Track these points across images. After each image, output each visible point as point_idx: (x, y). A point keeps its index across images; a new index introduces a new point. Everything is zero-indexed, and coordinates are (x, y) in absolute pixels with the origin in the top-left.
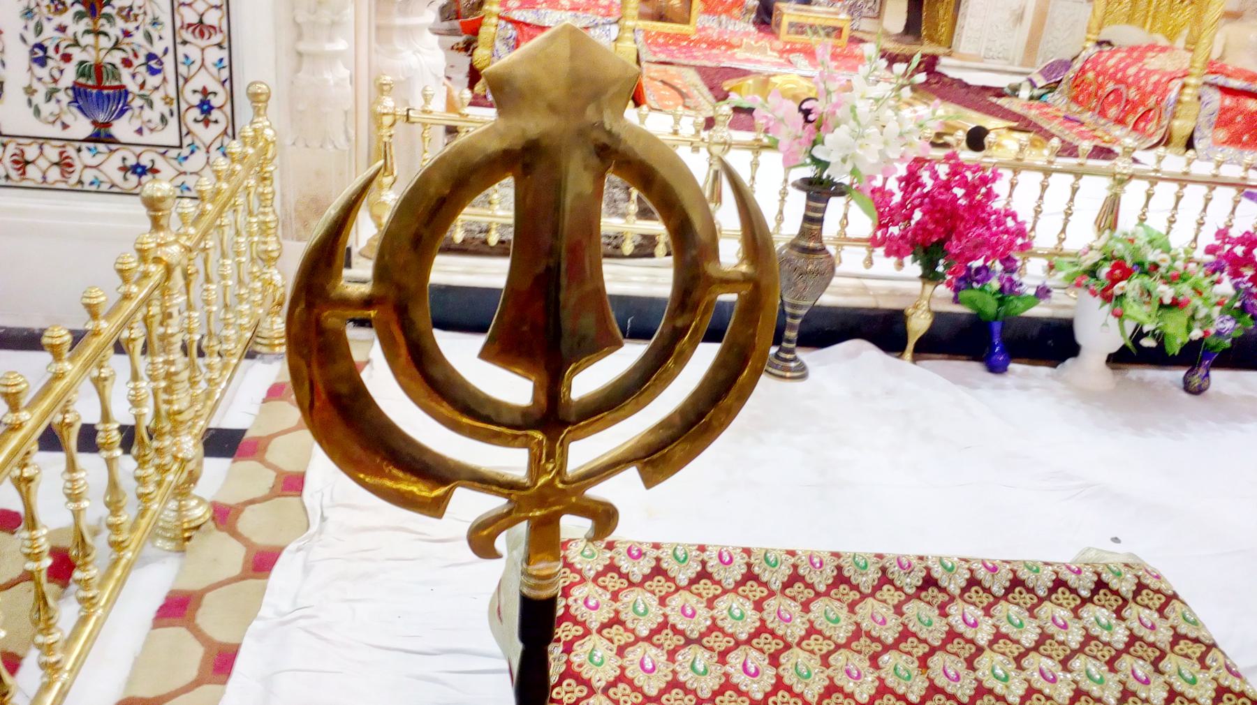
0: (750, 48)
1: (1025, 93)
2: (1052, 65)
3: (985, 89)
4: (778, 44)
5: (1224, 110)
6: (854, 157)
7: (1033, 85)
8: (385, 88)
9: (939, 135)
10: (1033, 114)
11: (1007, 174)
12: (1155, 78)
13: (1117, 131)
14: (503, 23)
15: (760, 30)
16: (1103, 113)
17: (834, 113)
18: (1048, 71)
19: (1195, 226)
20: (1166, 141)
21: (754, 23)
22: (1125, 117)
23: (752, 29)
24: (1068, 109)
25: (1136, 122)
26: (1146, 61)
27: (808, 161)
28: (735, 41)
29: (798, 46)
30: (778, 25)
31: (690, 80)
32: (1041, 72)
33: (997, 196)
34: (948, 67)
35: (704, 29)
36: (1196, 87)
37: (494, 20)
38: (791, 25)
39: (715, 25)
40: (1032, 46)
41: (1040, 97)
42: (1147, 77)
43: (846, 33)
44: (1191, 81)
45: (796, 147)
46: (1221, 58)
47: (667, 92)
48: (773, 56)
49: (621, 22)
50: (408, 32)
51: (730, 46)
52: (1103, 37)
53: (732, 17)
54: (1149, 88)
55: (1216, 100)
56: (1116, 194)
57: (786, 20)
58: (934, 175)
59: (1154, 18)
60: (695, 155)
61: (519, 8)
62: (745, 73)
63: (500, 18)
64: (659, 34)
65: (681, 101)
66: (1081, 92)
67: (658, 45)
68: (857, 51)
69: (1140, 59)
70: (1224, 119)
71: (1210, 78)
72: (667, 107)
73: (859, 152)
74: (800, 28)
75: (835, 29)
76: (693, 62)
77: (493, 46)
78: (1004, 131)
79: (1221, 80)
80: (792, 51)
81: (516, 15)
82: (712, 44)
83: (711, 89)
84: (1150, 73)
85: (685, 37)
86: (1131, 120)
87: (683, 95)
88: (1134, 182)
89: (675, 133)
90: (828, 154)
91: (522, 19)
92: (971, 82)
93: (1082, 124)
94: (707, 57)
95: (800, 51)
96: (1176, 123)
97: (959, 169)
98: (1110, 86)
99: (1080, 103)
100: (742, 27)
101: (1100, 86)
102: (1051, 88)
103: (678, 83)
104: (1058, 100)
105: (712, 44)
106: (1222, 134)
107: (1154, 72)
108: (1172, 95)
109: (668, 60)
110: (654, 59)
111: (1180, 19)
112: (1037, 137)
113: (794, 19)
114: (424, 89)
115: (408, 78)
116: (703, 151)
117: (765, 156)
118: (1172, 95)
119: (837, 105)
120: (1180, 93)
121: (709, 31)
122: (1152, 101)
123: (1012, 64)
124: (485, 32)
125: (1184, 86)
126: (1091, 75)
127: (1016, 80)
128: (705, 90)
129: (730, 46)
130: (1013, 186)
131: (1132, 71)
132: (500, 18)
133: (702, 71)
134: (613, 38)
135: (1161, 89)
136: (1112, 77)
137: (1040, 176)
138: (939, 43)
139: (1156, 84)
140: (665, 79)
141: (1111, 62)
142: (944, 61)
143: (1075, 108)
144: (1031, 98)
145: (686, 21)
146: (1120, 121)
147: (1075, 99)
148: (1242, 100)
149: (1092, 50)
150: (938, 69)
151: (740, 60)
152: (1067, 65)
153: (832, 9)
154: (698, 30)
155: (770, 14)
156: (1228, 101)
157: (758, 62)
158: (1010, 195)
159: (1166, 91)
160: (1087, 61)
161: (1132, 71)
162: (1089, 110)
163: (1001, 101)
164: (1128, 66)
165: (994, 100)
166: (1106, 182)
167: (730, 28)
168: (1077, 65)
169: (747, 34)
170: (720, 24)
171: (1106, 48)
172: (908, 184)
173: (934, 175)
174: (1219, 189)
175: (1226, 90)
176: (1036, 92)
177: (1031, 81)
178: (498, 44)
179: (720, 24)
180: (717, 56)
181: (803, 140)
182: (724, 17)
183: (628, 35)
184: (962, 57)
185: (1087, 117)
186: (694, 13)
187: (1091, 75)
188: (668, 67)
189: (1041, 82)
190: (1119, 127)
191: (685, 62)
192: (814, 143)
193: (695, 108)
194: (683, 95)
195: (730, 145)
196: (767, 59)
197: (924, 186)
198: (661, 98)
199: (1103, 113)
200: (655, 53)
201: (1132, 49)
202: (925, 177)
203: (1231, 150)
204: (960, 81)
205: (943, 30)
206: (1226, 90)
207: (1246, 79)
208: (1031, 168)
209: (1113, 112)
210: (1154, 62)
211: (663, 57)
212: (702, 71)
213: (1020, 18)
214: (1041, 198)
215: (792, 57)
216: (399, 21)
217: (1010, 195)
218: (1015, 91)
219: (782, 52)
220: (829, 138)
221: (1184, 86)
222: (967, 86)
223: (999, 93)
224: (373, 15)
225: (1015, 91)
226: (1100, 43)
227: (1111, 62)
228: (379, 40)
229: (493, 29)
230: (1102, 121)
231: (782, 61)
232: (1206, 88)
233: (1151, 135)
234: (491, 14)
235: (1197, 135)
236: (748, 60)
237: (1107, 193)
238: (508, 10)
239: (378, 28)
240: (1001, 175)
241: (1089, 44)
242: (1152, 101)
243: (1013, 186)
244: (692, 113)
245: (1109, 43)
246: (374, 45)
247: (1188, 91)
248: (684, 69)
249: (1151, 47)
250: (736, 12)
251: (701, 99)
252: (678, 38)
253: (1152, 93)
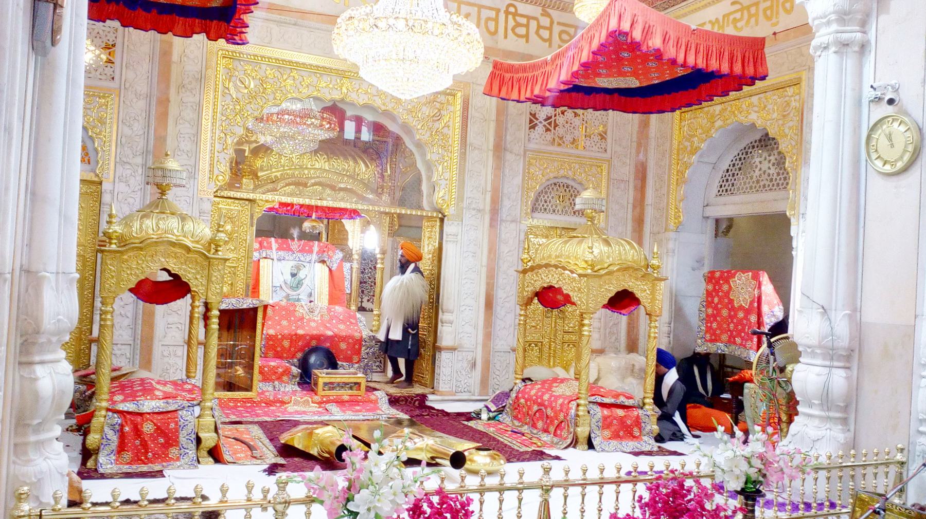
0: (297, 403)
1: (484, 416)
2: (498, 396)
3: (460, 414)
4: (316, 398)
5: (605, 418)
6: (375, 507)
7: (490, 411)
8: (22, 496)
9: (433, 458)
10: (491, 431)
11: (475, 497)
12: (560, 401)
13: (545, 438)
14: (110, 414)
15: (303, 389)
16: (534, 426)
17: (359, 477)
18: (497, 399)
19: (597, 512)
20: (574, 443)
21: (299, 384)
22: (548, 427)
23: (297, 388)
24: (513, 424)
25: (555, 430)
26: (554, 389)
27: (346, 512)
28: (286, 399)
29: (332, 398)
30: (316, 384)
31: (256, 434)
32: (492, 401)
33: (473, 512)
34: (434, 401)
35: (263, 392)
36: (585, 405)
37: (103, 412)
38: (325, 384)
39: (271, 389)
40: (484, 382)
41: (494, 418)
42: (556, 401)
43: (363, 387)
44: (582, 402)
45: (336, 505)
46: (597, 380)
47: (239, 446)
48: (314, 407)
49: (202, 404)
50: (40, 444)
51: (283, 403)
52: (525, 376)
53: (283, 382)
54: (558, 408)
55: (599, 412)
56: (546, 500)
57: (321, 382)
58: (431, 505)
59: (554, 357)
60: (264, 513)
61: (122, 401)
62: (296, 424)
63: (108, 410)
64: (230, 400)
65: (249, 453)
66: (518, 412)
67: (230, 408)
68: (373, 397)
69: (549, 389)
70: (606, 423)
71: (592, 399)
72: (239, 459)
73: (378, 505)
74: (331, 386)
75: (355, 383)
76: (256, 420)
77: (102, 431)
78: (474, 450)
79: (599, 399)
80: (328, 402)
81: (121, 407)
82: (269, 403)
83: (271, 440)
84: (557, 397)
85: (249, 400)
86: (552, 429)
87: (250, 447)
88: (555, 489)
89: (249, 500)
90: (358, 507)
91: (125, 409)
92: (449, 411)
93: (523, 435)
94: (266, 414)
95: (333, 401)
96: (579, 429)
97: (445, 500)
98: (535, 408)
99: (519, 420)
100: (290, 388)
101: (529, 408)
102: (500, 411)
103: (245, 437)
104: (506, 418)
105: (269, 403)
106: (607, 433)
107: (560, 396)
108: (573, 412)
109: (238, 419)
110: (227, 420)
111: (570, 356)
112: (495, 452)
113: (327, 380)
114: (55, 493)
115: (39, 480)
116: (270, 510)
117: (315, 507)
118: (573, 412)
119: (361, 471)
120: (577, 410)
121: (267, 394)
122: (561, 416)
123: (474, 395)
124: (96, 422)
125: (578, 405)
126: (522, 401)
127: (480, 405)
128: (267, 441)
129: (283, 403)
130: (481, 503)
131: (546, 397)
132: (108, 410)
133: (262, 424)
134: (196, 415)
135: (565, 409)
136: (535, 402)
137: (497, 494)
138: (425, 385)
139: (562, 405)
140: (237, 435)
141: (533, 392)
142: (430, 397)
143: (516, 423)
144: (489, 419)
145: (249, 389)
146: (546, 431)
147: (516, 418)
148: (614, 410)
149: (520, 385)
150: (428, 404)
151: (290, 413)
152: (507, 395)
153: (352, 370)
154: (259, 394)
155: (310, 377)
156: (606, 412)
157: (304, 413)
158: (481, 510)
159: (569, 409)
160: (518, 393)
161: (546, 397)
162: (526, 424)
163: (471, 424)
164: (543, 394)
165: (466, 423)
166: (538, 492)
167: (282, 389)
168: (513, 395)
169: (294, 392)
170: (274, 387)
171: (529, 383)
172: (414, 513)
173: (431, 505)
174: (606, 486)
175: (603, 405)
176: (491, 415)
177: (487, 407)
178: (106, 429)
179: (274, 387)
180: (273, 412)
181: (340, 499)
182: (276, 383)
183: (208, 412)
184: (442, 394)
185: (525, 429)
186: (255, 382)
187: (522, 401)
188: (238, 426)
189: (493, 408)
190: (545, 435)
191: (250, 420)
192: (348, 500)
193: (261, 458)
194: (250, 447)
195: (289, 503)
196: (310, 409)
197: (425, 513)
198: (236, 452)
199: (534, 426)
200: (227, 415)
201: (544, 382)
202: (425, 507)
203: (614, 443)
204: (443, 411)
205: (428, 377)
206: (603, 405)
207: (613, 397)
208: (490, 490)
209: (540, 424)
210: (559, 390)
211: (233, 418)
212: (262, 424)
213: (474, 365)
214: (500, 509)
215: (328, 406)
216: (33, 438)
217: (481, 510)
218: (478, 415)
219: (320, 403)
220: (357, 497)
221: (578, 405)
222: (447, 414)
223: (468, 416)
224: (12, 434)
225: (478, 415)
226: (524, 380)
227: (533, 392)
228: (16, 454)
229: (102, 419)
230: (535, 431)
231: (320, 410)
232: (591, 405)
233: (565, 439)
234: (101, 408)
235: (593, 435)
236: (297, 412)
237: (540, 499)
238: (114, 403)
239: (15, 445)
240: (472, 500)
241: (518, 381)
242: (561, 416)
243: (481, 503)
244: (259, 462)
245: (530, 379)
246: (13, 458)
247: (581, 408)
248: (250, 426)
249: (555, 380)
250: (285, 378)
251: (265, 449)
252: (246, 401)
253: (561, 410)
